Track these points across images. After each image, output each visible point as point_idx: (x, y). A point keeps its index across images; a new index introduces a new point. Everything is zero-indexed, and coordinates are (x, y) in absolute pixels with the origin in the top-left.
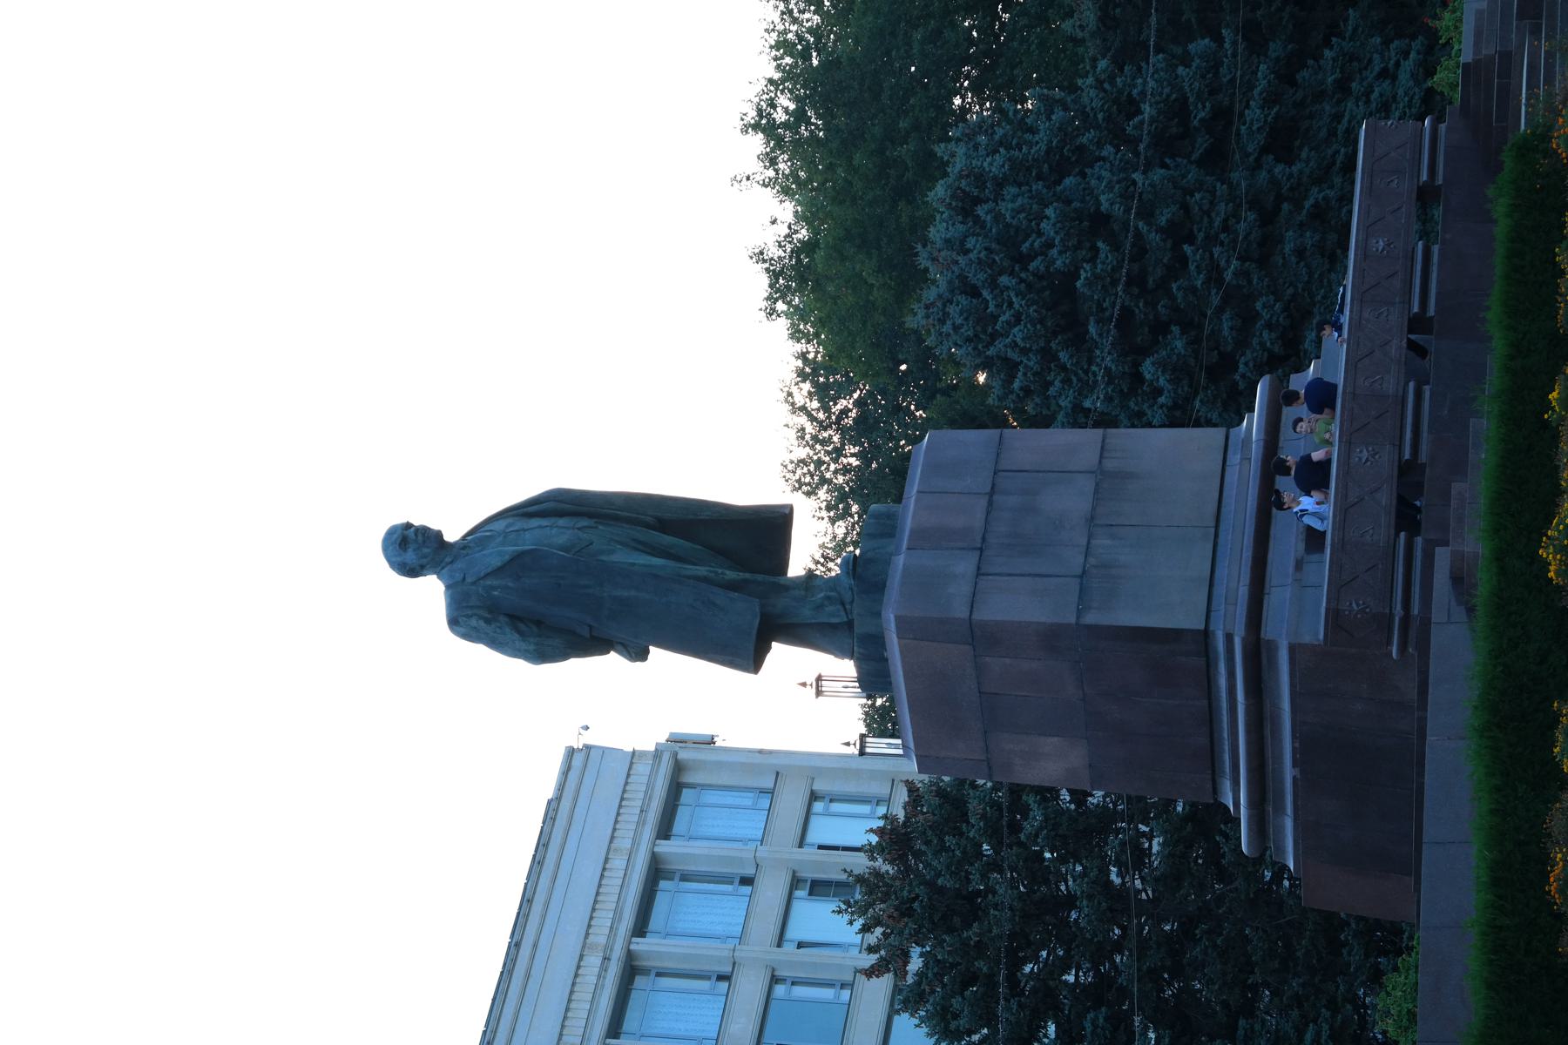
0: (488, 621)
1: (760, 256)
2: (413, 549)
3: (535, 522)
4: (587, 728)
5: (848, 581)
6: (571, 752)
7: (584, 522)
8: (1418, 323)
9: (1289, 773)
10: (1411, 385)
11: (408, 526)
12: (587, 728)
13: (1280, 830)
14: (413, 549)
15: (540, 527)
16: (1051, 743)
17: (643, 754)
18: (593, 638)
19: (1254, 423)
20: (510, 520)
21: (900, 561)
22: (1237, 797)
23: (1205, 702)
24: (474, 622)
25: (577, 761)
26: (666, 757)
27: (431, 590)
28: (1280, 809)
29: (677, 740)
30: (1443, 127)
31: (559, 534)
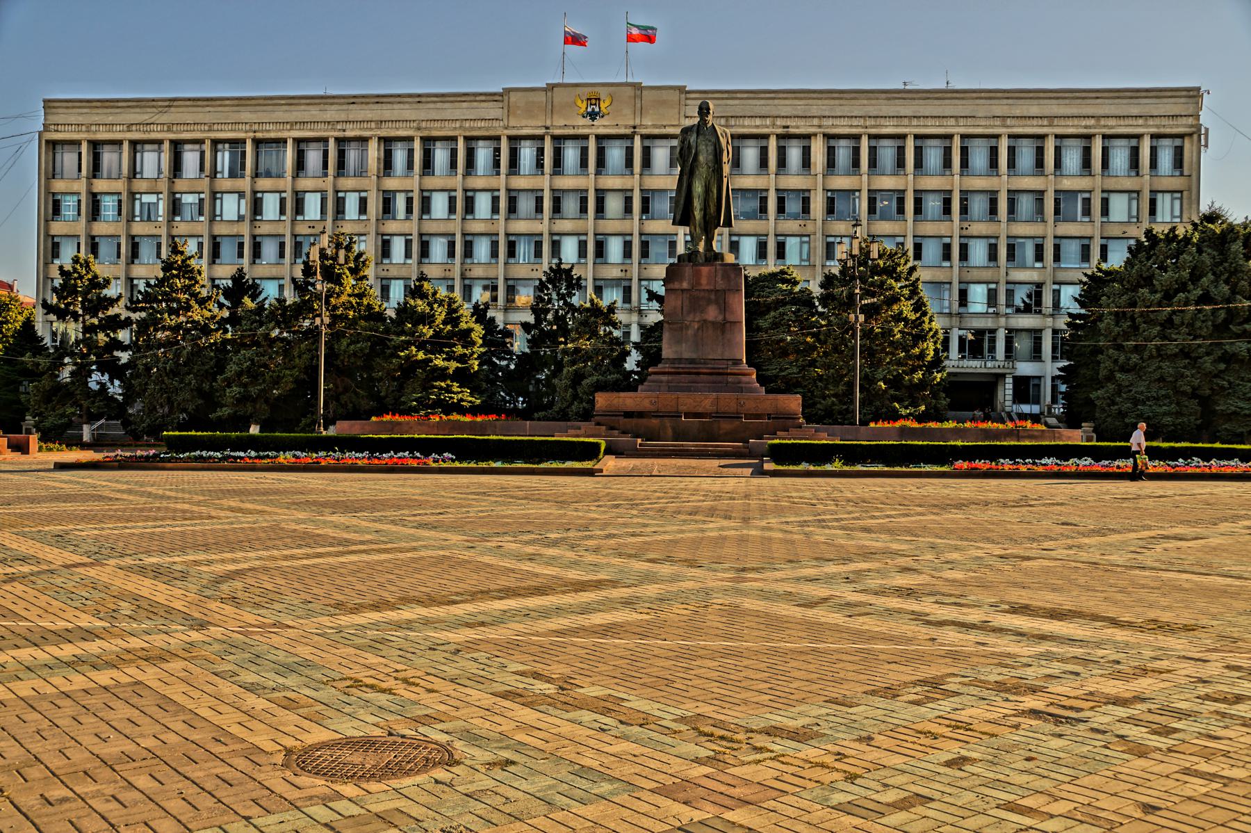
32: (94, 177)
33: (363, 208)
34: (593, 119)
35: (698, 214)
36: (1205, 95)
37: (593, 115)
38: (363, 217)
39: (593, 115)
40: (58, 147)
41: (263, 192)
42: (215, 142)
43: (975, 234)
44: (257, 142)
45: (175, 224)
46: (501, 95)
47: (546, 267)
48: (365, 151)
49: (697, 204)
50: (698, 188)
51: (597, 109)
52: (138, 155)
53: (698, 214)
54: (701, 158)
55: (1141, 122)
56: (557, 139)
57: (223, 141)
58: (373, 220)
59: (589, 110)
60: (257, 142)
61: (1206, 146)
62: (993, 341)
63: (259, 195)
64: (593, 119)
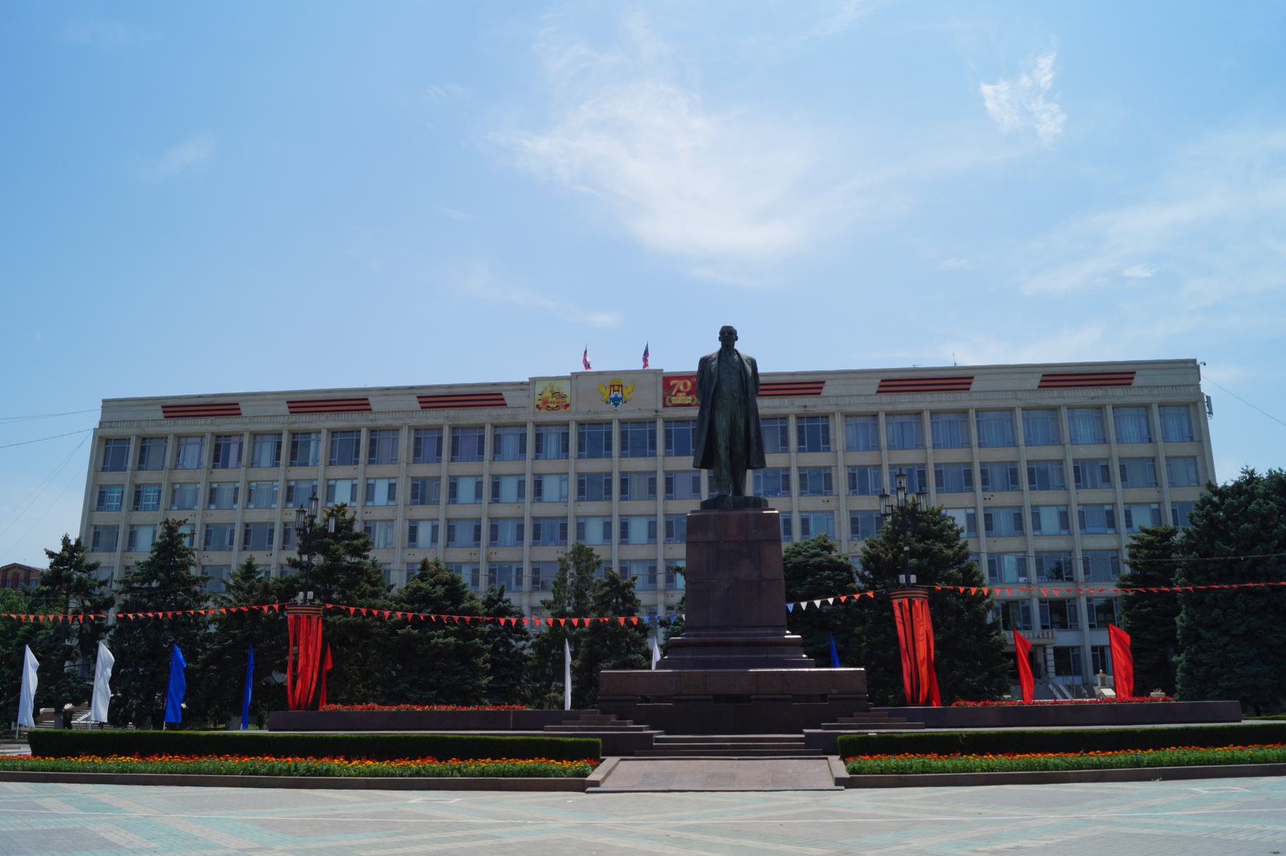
2: (728, 336)
6: (1194, 361)
14: (728, 336)
27: (714, 347)
32: (140, 469)
33: (391, 495)
34: (616, 405)
35: (723, 453)
36: (1202, 367)
37: (616, 401)
38: (391, 503)
39: (616, 401)
40: (258, 438)
41: (336, 480)
42: (255, 435)
43: (999, 504)
44: (1115, 407)
45: (210, 512)
46: (527, 384)
47: (570, 549)
48: (396, 440)
49: (722, 441)
50: (722, 423)
51: (620, 395)
52: (258, 446)
53: (723, 453)
54: (725, 388)
55: (1146, 391)
56: (583, 424)
57: (263, 434)
58: (401, 505)
59: (613, 396)
60: (1115, 407)
61: (1211, 413)
62: (1043, 618)
63: (332, 483)
64: (616, 405)
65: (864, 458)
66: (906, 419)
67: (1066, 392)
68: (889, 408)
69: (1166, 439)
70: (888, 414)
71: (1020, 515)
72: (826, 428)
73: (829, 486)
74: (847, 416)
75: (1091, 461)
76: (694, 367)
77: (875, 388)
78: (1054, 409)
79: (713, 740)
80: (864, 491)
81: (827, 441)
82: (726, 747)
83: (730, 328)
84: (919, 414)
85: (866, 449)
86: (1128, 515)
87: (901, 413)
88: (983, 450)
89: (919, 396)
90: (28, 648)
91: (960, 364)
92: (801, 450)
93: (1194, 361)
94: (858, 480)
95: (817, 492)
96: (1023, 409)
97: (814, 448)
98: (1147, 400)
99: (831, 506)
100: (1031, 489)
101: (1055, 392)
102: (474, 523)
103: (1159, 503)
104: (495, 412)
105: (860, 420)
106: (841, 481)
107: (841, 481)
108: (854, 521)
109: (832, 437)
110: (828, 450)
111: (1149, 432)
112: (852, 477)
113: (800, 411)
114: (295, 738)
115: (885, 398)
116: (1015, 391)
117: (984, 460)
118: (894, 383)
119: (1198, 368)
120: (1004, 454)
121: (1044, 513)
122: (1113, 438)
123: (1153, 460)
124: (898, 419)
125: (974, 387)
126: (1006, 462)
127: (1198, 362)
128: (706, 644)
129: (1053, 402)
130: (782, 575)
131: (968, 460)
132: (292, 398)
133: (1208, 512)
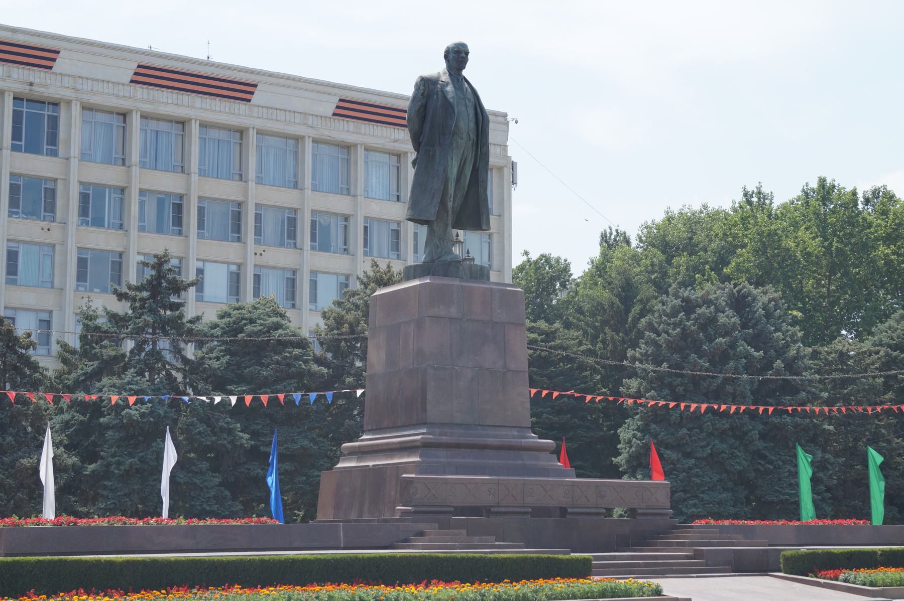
0: (423, 94)
1: (807, 184)
2: (457, 57)
3: (471, 112)
4: (516, 122)
5: (448, 258)
6: (505, 115)
7: (473, 136)
8: (563, 511)
9: (371, 464)
10: (530, 510)
11: (467, 53)
12: (516, 122)
13: (350, 460)
14: (457, 57)
15: (468, 115)
16: (383, 355)
17: (506, 150)
18: (420, 143)
19: (533, 439)
20: (472, 100)
21: (456, 282)
22: (367, 439)
23: (400, 424)
24: (422, 88)
25: (501, 119)
26: (504, 162)
27: (437, 68)
28: (359, 459)
29: (513, 165)
30: (603, 517)
31: (466, 124)
36: (512, 124)
43: (272, 263)
65: (107, 175)
66: (163, 126)
67: (365, 127)
68: (148, 108)
69: (260, 181)
70: (145, 116)
71: (293, 281)
72: (54, 121)
73: (51, 207)
74: (87, 108)
75: (381, 221)
76: (408, 90)
77: (128, 76)
78: (348, 147)
79: (614, 558)
80: (98, 222)
81: (53, 139)
82: (639, 565)
83: (464, 46)
84: (183, 123)
85: (107, 160)
86: (314, 284)
87: (159, 118)
88: (261, 187)
89: (186, 98)
90: (799, 449)
91: (216, 58)
92: (15, 148)
93: (505, 115)
94: (90, 205)
95: (32, 213)
96: (315, 141)
97: (33, 148)
98: (124, 104)
99: (54, 236)
100: (313, 248)
101: (352, 125)
102: (342, 279)
103: (181, 259)
104: (35, 75)
105: (101, 117)
106: (69, 202)
107: (69, 202)
108: (82, 263)
109: (62, 135)
110: (54, 153)
111: (296, 176)
112: (84, 198)
113: (22, 89)
114: (382, 558)
115: (141, 92)
116: (304, 114)
117: (367, 215)
118: (155, 74)
119: (507, 124)
120: (285, 198)
121: (321, 279)
122: (308, 182)
123: (122, 190)
124: (153, 125)
125: (256, 99)
126: (284, 208)
127: (509, 118)
128: (458, 446)
129: (350, 138)
130: (525, 367)
131: (239, 198)
132: (147, 61)
133: (681, 320)
